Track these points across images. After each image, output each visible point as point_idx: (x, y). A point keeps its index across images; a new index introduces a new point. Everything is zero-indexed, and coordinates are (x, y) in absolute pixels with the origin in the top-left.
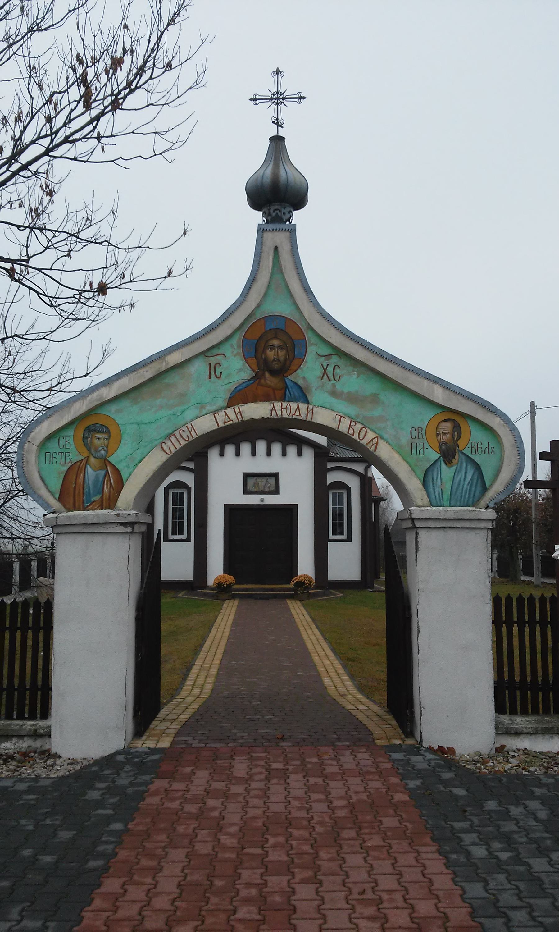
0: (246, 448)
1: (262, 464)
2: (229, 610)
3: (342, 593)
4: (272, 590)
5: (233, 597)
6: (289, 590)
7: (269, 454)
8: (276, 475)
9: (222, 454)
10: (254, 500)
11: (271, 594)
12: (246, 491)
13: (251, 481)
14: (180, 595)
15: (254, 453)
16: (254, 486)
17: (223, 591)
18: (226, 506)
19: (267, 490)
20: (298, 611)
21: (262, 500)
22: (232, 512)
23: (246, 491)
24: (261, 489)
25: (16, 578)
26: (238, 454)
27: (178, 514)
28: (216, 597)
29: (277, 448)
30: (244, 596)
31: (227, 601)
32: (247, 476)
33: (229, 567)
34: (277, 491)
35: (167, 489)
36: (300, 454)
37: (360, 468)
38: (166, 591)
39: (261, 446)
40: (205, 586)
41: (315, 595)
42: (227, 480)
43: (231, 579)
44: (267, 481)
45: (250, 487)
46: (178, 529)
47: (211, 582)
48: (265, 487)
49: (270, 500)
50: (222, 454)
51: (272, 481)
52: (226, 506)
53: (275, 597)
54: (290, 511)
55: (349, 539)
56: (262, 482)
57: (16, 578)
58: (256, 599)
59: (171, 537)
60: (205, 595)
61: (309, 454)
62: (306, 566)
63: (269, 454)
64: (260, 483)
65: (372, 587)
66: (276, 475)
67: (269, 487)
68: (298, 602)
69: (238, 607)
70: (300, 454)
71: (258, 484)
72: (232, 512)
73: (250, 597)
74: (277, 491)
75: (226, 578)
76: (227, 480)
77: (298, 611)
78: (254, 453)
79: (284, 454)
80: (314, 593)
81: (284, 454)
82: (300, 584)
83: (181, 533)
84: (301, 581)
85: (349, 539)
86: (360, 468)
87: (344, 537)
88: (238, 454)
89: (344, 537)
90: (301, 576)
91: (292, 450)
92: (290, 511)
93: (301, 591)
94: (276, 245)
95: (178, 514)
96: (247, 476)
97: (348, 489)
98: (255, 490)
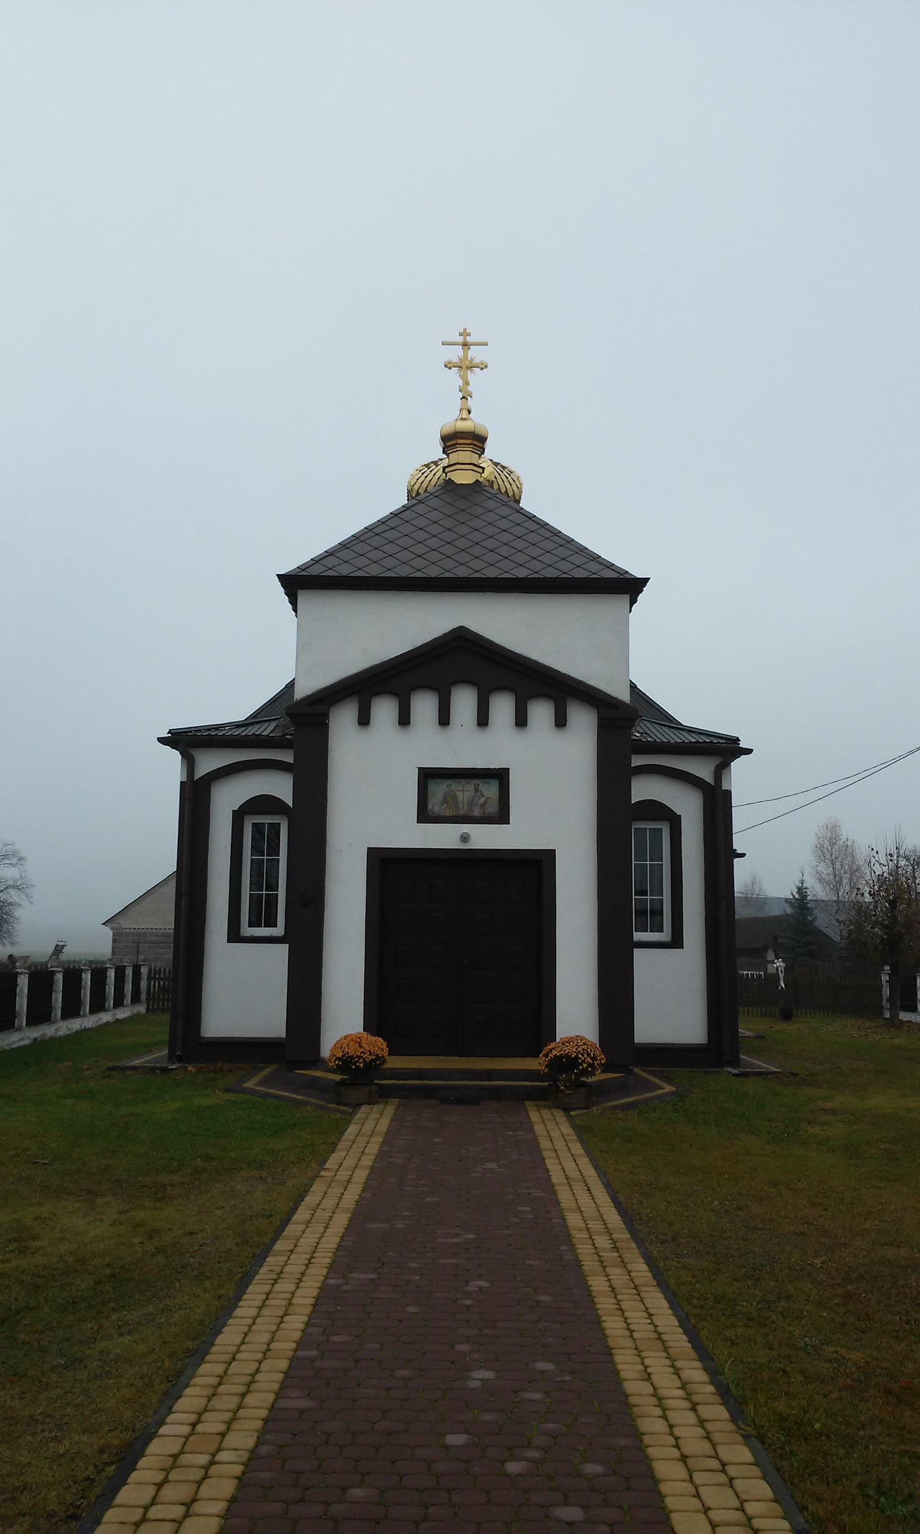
0: (424, 706)
1: (464, 745)
2: (368, 1131)
3: (668, 1079)
4: (490, 1075)
5: (384, 1094)
6: (531, 1075)
7: (483, 720)
8: (501, 776)
9: (364, 720)
10: (443, 837)
11: (487, 1088)
12: (424, 816)
13: (438, 790)
14: (249, 1084)
15: (444, 720)
16: (445, 801)
17: (358, 1079)
18: (372, 852)
19: (477, 813)
20: (569, 1166)
21: (465, 838)
22: (385, 865)
23: (424, 816)
24: (463, 810)
25: (22, 1003)
26: (404, 720)
27: (264, 877)
28: (335, 1093)
29: (502, 707)
30: (413, 1093)
31: (364, 1109)
32: (427, 776)
33: (378, 1013)
34: (502, 816)
35: (238, 816)
36: (561, 722)
37: (703, 769)
38: (226, 1067)
39: (464, 701)
40: (315, 1061)
41: (602, 1091)
42: (375, 792)
43: (378, 1045)
44: (477, 790)
45: (434, 806)
46: (263, 913)
47: (328, 1046)
48: (471, 804)
49: (486, 837)
50: (364, 720)
51: (491, 790)
52: (372, 852)
53: (497, 1094)
54: (538, 867)
55: (676, 942)
56: (464, 792)
57: (22, 1003)
58: (445, 1101)
59: (247, 931)
60: (312, 1085)
61: (583, 724)
62: (575, 1012)
63: (483, 720)
64: (459, 794)
65: (736, 1063)
66: (501, 776)
67: (483, 806)
68: (560, 1116)
69: (389, 1138)
70: (561, 722)
71: (455, 798)
72: (385, 865)
73: (428, 1093)
74: (502, 816)
75: (364, 1044)
76: (375, 792)
77: (557, 1140)
78: (444, 720)
79: (521, 721)
80: (600, 1084)
81: (521, 721)
82: (566, 1064)
83: (271, 923)
84: (567, 1056)
85: (676, 942)
86: (703, 769)
87: (664, 936)
88: (404, 720)
89: (664, 936)
90: (567, 1041)
91: (541, 713)
92: (538, 867)
93: (565, 1083)
94: (458, 839)
95: (264, 877)
96: (427, 776)
97: (674, 821)
98: (448, 813)
